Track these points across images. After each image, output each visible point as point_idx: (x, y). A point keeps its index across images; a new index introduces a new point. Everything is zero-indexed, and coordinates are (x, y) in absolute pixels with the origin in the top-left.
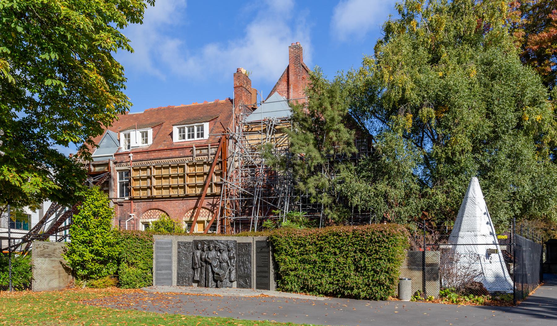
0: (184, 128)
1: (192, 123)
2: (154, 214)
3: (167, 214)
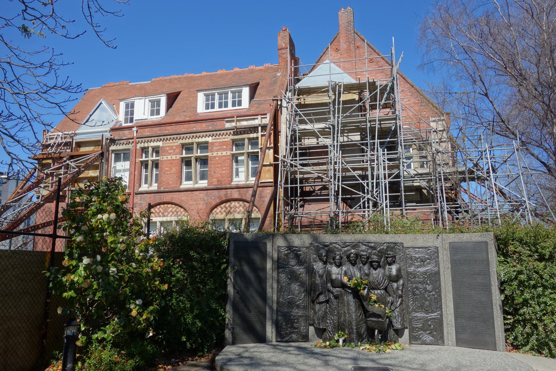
0: (213, 95)
1: (225, 88)
2: (166, 210)
3: (185, 209)
